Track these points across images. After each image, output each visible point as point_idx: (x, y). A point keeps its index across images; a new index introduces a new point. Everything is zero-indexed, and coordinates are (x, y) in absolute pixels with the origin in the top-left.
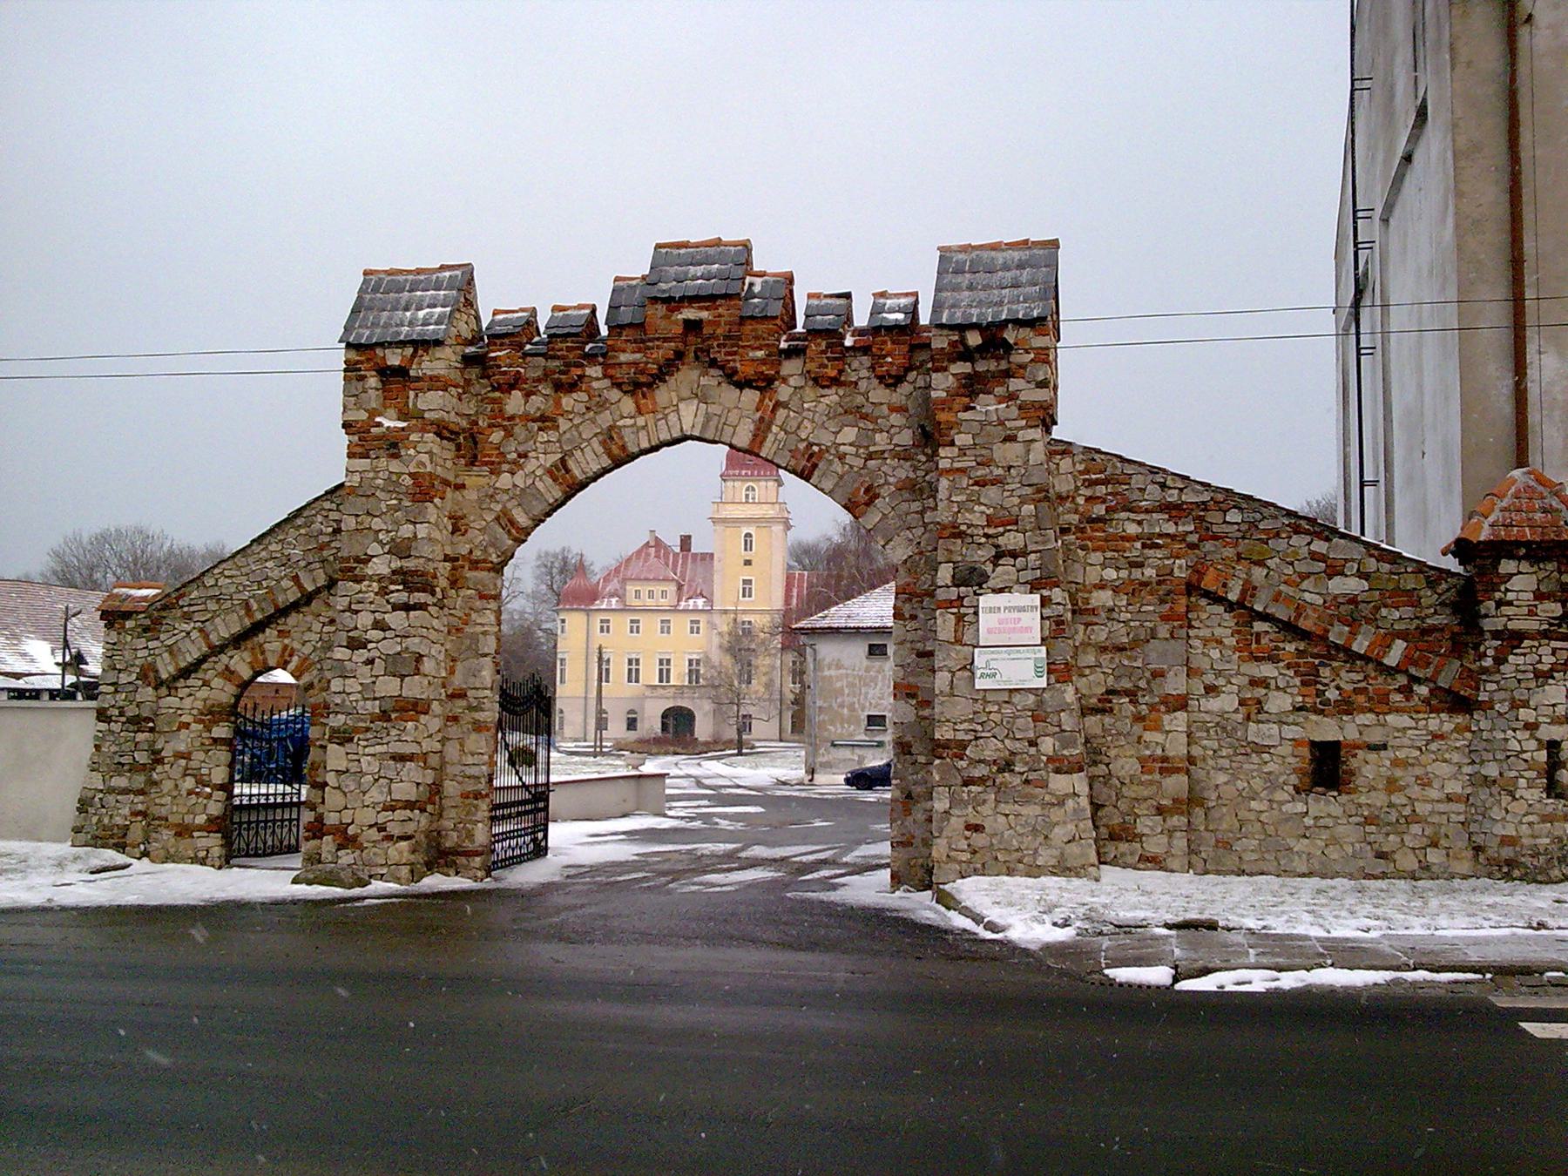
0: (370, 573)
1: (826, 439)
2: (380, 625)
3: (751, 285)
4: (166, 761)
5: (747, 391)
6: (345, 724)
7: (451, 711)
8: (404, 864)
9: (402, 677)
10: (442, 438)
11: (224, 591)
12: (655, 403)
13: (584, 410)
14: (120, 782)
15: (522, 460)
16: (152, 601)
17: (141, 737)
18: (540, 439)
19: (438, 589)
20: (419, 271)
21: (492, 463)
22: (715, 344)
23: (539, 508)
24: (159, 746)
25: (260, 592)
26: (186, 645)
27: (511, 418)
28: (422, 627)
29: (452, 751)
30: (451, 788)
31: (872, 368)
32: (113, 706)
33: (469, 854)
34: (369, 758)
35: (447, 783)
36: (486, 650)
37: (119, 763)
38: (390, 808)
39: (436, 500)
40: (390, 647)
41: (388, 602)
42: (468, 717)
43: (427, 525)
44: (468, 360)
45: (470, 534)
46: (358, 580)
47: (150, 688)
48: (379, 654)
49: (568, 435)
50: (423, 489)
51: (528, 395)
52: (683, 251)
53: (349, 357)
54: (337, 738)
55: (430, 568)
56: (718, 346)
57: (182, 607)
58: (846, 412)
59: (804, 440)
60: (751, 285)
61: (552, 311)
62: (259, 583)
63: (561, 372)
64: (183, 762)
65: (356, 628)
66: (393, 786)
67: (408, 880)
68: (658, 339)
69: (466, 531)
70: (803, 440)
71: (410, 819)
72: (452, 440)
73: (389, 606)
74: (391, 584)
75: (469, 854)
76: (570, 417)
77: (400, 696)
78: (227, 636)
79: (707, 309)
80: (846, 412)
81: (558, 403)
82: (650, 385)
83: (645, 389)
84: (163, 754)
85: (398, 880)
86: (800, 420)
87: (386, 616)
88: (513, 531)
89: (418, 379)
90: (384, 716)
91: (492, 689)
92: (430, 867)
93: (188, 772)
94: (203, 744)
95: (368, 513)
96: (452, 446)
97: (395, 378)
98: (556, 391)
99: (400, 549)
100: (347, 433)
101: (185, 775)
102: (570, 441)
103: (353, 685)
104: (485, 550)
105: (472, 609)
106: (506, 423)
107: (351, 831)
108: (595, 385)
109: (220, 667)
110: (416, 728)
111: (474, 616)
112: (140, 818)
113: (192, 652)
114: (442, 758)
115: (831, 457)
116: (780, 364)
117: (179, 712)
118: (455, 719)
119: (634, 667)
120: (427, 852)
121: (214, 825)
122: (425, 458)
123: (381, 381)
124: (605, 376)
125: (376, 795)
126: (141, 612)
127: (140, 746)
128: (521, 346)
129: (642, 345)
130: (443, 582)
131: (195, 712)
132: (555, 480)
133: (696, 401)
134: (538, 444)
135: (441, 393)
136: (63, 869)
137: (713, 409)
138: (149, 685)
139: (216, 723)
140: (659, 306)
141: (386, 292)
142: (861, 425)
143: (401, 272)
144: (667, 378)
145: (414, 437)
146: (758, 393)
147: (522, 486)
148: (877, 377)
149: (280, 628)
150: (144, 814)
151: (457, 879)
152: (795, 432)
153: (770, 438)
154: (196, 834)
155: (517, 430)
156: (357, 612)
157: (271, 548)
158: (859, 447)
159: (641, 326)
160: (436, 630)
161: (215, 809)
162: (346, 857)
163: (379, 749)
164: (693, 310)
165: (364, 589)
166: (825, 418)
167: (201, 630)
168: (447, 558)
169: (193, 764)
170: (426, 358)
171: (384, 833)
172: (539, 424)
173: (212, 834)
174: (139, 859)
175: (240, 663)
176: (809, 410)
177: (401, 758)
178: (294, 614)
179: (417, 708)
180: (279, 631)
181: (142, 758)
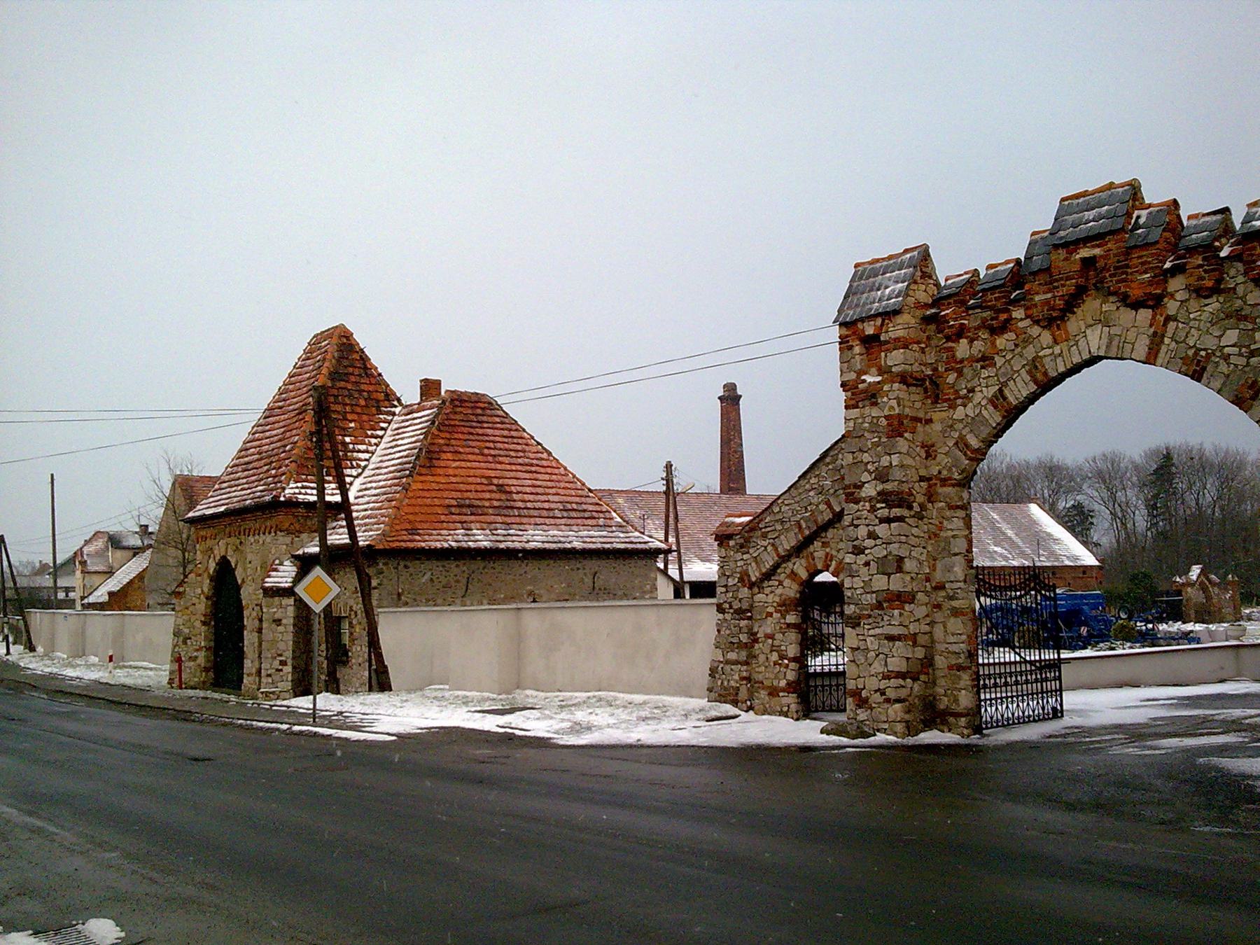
0: (864, 496)
1: (1210, 343)
2: (872, 535)
3: (1138, 217)
4: (760, 640)
5: (1141, 311)
6: (855, 612)
7: (935, 600)
8: (899, 722)
9: (889, 575)
10: (908, 385)
11: (785, 515)
12: (1067, 332)
13: (1013, 347)
14: (732, 656)
15: (971, 395)
16: (744, 525)
17: (743, 623)
18: (982, 376)
19: (915, 504)
20: (890, 258)
21: (949, 399)
22: (1107, 275)
23: (985, 432)
24: (755, 630)
25: (807, 514)
26: (765, 556)
27: (962, 361)
28: (900, 535)
29: (938, 632)
30: (940, 661)
31: (1246, 273)
32: (725, 602)
33: (958, 715)
34: (872, 638)
35: (937, 658)
36: (956, 550)
37: (731, 642)
38: (886, 677)
39: (906, 435)
40: (880, 552)
41: (876, 516)
42: (947, 605)
43: (898, 455)
44: (926, 320)
45: (940, 457)
46: (857, 502)
47: (746, 589)
48: (872, 558)
49: (1003, 370)
50: (897, 427)
51: (971, 341)
52: (1081, 200)
53: (842, 333)
54: (851, 623)
55: (905, 488)
56: (1110, 276)
57: (761, 529)
58: (1227, 317)
59: (1192, 347)
60: (1138, 217)
61: (987, 269)
62: (806, 508)
63: (992, 319)
64: (770, 641)
65: (857, 539)
66: (888, 659)
67: (904, 734)
68: (1061, 279)
69: (936, 456)
70: (1191, 347)
71: (903, 687)
72: (921, 386)
73: (877, 520)
74: (877, 503)
75: (958, 715)
76: (1004, 354)
77: (888, 589)
78: (789, 548)
79: (1098, 246)
80: (1227, 317)
81: (993, 344)
82: (1062, 318)
83: (1059, 322)
84: (758, 636)
85: (895, 734)
86: (1188, 329)
87: (876, 528)
88: (969, 452)
89: (887, 342)
90: (879, 606)
91: (965, 581)
92: (928, 725)
93: (774, 648)
94: (781, 628)
95: (861, 450)
96: (920, 390)
97: (871, 342)
98: (991, 336)
99: (882, 476)
100: (844, 391)
101: (771, 651)
102: (1004, 374)
103: (858, 583)
104: (950, 470)
105: (943, 518)
106: (957, 366)
107: (864, 694)
108: (1021, 324)
109: (788, 571)
110: (901, 615)
111: (945, 523)
112: (745, 682)
113: (769, 561)
114: (932, 637)
115: (1217, 360)
116: (1166, 282)
117: (766, 605)
118: (938, 606)
120: (923, 712)
121: (792, 687)
122: (894, 403)
123: (865, 347)
124: (1027, 317)
125: (878, 667)
126: (737, 535)
127: (743, 630)
128: (964, 303)
129: (1050, 285)
130: (920, 498)
131: (775, 604)
132: (995, 407)
133: (1100, 326)
134: (981, 380)
135: (902, 351)
136: (687, 718)
137: (1114, 331)
138: (745, 586)
139: (787, 612)
140: (1060, 251)
141: (867, 279)
142: (1241, 327)
143: (877, 261)
144: (1075, 310)
145: (886, 388)
146: (1150, 310)
147: (972, 415)
148: (1252, 280)
149: (823, 540)
150: (748, 679)
151: (949, 735)
152: (1184, 341)
153: (1164, 349)
154: (781, 694)
155: (965, 370)
156: (857, 526)
157: (812, 482)
158: (1240, 347)
159: (1047, 270)
160: (915, 537)
161: (791, 676)
162: (863, 715)
163: (878, 631)
164: (1087, 249)
165: (861, 509)
166: (1209, 325)
167: (773, 545)
168: (922, 479)
169: (776, 643)
170: (891, 325)
171: (884, 697)
172: (982, 363)
173: (790, 695)
174: (747, 711)
175: (799, 567)
176: (1195, 319)
177: (891, 638)
178: (831, 530)
179: (909, 598)
180: (823, 543)
181: (744, 638)
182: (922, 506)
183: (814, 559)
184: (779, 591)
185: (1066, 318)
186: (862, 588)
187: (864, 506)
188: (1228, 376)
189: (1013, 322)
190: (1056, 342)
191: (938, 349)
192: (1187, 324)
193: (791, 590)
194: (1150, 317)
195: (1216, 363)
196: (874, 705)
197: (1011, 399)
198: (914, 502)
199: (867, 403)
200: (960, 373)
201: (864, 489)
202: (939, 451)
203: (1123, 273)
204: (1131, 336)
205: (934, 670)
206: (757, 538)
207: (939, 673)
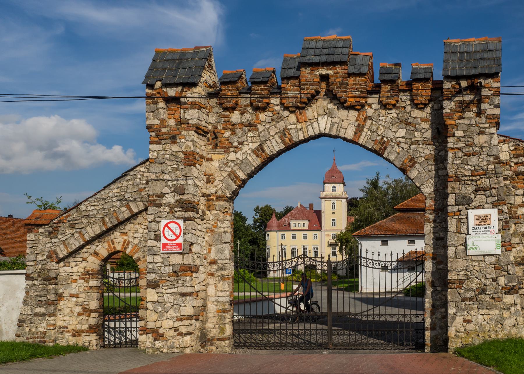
1: (391, 135)
12: (305, 117)
13: (271, 121)
15: (241, 146)
19: (200, 211)
21: (225, 147)
22: (335, 87)
27: (234, 125)
34: (168, 295)
36: (226, 241)
42: (219, 273)
45: (216, 183)
49: (263, 133)
51: (242, 114)
54: (152, 285)
69: (213, 182)
70: (379, 135)
71: (191, 325)
72: (205, 136)
86: (378, 125)
88: (237, 181)
89: (185, 103)
105: (218, 220)
109: (92, 251)
111: (219, 224)
113: (75, 244)
117: (71, 274)
119: (334, 250)
132: (257, 156)
134: (248, 138)
135: (197, 110)
137: (336, 120)
142: (408, 128)
146: (357, 112)
147: (241, 159)
153: (364, 134)
163: (173, 290)
166: (390, 125)
167: (80, 233)
173: (91, 334)
182: (204, 212)
183: (113, 244)
184: (84, 264)
185: (306, 109)
186: (162, 262)
187: (164, 209)
188: (398, 154)
189: (271, 105)
190: (298, 121)
191: (218, 115)
192: (378, 122)
193: (93, 263)
194: (356, 116)
195: (392, 145)
196: (168, 338)
197: (268, 152)
198: (200, 209)
199: (168, 141)
200: (233, 132)
201: (164, 198)
202: (216, 179)
203: (344, 88)
204: (345, 124)
205: (207, 313)
206: (65, 227)
207: (210, 315)
